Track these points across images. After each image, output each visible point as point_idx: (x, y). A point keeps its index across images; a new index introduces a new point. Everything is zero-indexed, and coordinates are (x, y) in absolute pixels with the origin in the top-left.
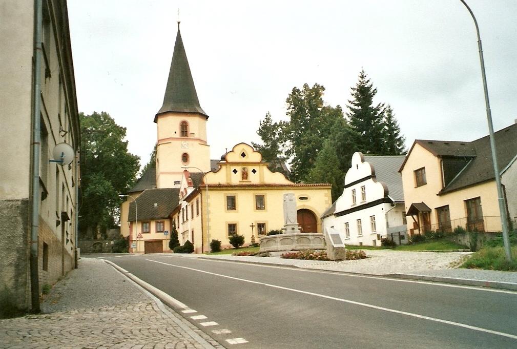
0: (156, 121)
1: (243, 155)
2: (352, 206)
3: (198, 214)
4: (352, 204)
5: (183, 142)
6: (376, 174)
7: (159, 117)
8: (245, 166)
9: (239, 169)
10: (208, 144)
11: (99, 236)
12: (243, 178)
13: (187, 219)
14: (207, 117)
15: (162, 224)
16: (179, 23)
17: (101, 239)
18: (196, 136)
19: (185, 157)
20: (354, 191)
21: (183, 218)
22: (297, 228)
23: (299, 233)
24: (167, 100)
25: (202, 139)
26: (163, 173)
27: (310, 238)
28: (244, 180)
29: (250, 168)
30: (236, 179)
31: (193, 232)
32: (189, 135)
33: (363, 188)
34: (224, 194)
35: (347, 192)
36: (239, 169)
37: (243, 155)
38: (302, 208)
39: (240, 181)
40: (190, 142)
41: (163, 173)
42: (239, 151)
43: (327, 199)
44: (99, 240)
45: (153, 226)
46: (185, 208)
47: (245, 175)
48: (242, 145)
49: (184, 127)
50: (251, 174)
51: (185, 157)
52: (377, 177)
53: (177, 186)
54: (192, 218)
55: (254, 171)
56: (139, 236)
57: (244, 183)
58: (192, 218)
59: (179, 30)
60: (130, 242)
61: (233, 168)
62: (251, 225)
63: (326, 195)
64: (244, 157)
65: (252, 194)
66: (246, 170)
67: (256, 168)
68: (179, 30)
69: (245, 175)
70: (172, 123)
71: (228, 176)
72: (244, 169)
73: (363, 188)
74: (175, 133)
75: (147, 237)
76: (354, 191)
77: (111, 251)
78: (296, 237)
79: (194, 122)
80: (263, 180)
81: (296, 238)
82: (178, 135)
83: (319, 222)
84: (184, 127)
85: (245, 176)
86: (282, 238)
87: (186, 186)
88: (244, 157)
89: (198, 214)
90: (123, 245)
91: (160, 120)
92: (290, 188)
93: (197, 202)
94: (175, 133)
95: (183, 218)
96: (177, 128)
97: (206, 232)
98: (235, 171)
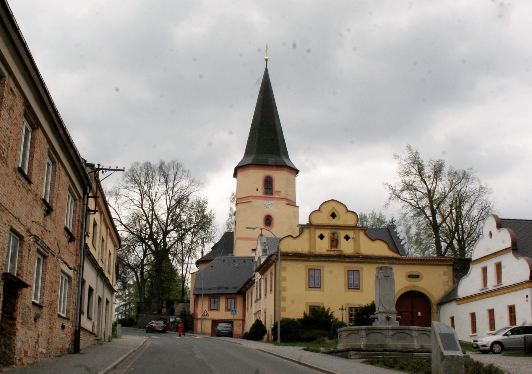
0: (235, 175)
1: (333, 216)
2: (481, 290)
3: (271, 290)
4: (482, 287)
5: (265, 201)
6: (518, 246)
7: (238, 171)
8: (335, 231)
9: (326, 233)
10: (297, 205)
11: (164, 310)
12: (332, 246)
13: (260, 297)
14: (296, 172)
15: (233, 300)
16: (267, 60)
17: (165, 314)
18: (283, 195)
19: (268, 220)
20: (485, 270)
21: (257, 295)
22: (394, 317)
23: (397, 325)
24: (248, 152)
25: (289, 198)
26: (239, 238)
27: (414, 334)
28: (333, 249)
29: (342, 234)
30: (323, 247)
31: (265, 312)
32: (274, 192)
33: (499, 266)
34: (345, 267)
35: (475, 272)
36: (326, 233)
37: (333, 216)
38: (412, 290)
39: (327, 250)
40: (275, 202)
41: (239, 238)
42: (327, 212)
43: (446, 278)
44: (163, 315)
45: (222, 303)
46: (259, 282)
47: (334, 242)
48: (332, 203)
49: (268, 183)
50: (342, 240)
51: (268, 220)
52: (519, 250)
53: (253, 255)
54: (266, 295)
55: (347, 238)
56: (205, 314)
57: (332, 253)
58: (266, 295)
59: (266, 70)
60: (195, 320)
61: (318, 232)
62: (341, 307)
63: (445, 273)
64: (334, 218)
65: (304, 266)
66: (336, 235)
67: (351, 234)
68: (266, 70)
69: (334, 242)
70: (257, 176)
71: (312, 243)
72: (333, 234)
73: (499, 266)
74: (257, 190)
75: (214, 315)
76: (485, 270)
77: (175, 330)
78: (390, 331)
79: (279, 177)
80: (315, 249)
81: (391, 333)
82: (260, 193)
83: (434, 308)
84: (268, 183)
85: (335, 243)
86: (349, 332)
87: (261, 254)
88: (334, 218)
89: (271, 290)
90: (188, 325)
91: (239, 174)
92: (395, 261)
93: (271, 273)
94: (257, 190)
95: (257, 295)
96: (260, 185)
97: (277, 313)
98: (321, 237)
